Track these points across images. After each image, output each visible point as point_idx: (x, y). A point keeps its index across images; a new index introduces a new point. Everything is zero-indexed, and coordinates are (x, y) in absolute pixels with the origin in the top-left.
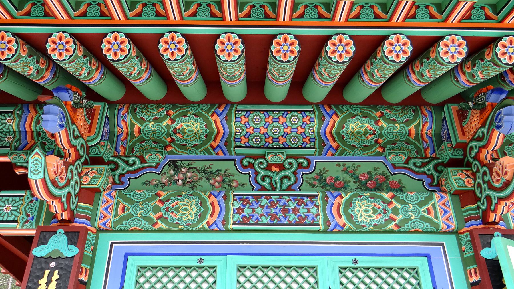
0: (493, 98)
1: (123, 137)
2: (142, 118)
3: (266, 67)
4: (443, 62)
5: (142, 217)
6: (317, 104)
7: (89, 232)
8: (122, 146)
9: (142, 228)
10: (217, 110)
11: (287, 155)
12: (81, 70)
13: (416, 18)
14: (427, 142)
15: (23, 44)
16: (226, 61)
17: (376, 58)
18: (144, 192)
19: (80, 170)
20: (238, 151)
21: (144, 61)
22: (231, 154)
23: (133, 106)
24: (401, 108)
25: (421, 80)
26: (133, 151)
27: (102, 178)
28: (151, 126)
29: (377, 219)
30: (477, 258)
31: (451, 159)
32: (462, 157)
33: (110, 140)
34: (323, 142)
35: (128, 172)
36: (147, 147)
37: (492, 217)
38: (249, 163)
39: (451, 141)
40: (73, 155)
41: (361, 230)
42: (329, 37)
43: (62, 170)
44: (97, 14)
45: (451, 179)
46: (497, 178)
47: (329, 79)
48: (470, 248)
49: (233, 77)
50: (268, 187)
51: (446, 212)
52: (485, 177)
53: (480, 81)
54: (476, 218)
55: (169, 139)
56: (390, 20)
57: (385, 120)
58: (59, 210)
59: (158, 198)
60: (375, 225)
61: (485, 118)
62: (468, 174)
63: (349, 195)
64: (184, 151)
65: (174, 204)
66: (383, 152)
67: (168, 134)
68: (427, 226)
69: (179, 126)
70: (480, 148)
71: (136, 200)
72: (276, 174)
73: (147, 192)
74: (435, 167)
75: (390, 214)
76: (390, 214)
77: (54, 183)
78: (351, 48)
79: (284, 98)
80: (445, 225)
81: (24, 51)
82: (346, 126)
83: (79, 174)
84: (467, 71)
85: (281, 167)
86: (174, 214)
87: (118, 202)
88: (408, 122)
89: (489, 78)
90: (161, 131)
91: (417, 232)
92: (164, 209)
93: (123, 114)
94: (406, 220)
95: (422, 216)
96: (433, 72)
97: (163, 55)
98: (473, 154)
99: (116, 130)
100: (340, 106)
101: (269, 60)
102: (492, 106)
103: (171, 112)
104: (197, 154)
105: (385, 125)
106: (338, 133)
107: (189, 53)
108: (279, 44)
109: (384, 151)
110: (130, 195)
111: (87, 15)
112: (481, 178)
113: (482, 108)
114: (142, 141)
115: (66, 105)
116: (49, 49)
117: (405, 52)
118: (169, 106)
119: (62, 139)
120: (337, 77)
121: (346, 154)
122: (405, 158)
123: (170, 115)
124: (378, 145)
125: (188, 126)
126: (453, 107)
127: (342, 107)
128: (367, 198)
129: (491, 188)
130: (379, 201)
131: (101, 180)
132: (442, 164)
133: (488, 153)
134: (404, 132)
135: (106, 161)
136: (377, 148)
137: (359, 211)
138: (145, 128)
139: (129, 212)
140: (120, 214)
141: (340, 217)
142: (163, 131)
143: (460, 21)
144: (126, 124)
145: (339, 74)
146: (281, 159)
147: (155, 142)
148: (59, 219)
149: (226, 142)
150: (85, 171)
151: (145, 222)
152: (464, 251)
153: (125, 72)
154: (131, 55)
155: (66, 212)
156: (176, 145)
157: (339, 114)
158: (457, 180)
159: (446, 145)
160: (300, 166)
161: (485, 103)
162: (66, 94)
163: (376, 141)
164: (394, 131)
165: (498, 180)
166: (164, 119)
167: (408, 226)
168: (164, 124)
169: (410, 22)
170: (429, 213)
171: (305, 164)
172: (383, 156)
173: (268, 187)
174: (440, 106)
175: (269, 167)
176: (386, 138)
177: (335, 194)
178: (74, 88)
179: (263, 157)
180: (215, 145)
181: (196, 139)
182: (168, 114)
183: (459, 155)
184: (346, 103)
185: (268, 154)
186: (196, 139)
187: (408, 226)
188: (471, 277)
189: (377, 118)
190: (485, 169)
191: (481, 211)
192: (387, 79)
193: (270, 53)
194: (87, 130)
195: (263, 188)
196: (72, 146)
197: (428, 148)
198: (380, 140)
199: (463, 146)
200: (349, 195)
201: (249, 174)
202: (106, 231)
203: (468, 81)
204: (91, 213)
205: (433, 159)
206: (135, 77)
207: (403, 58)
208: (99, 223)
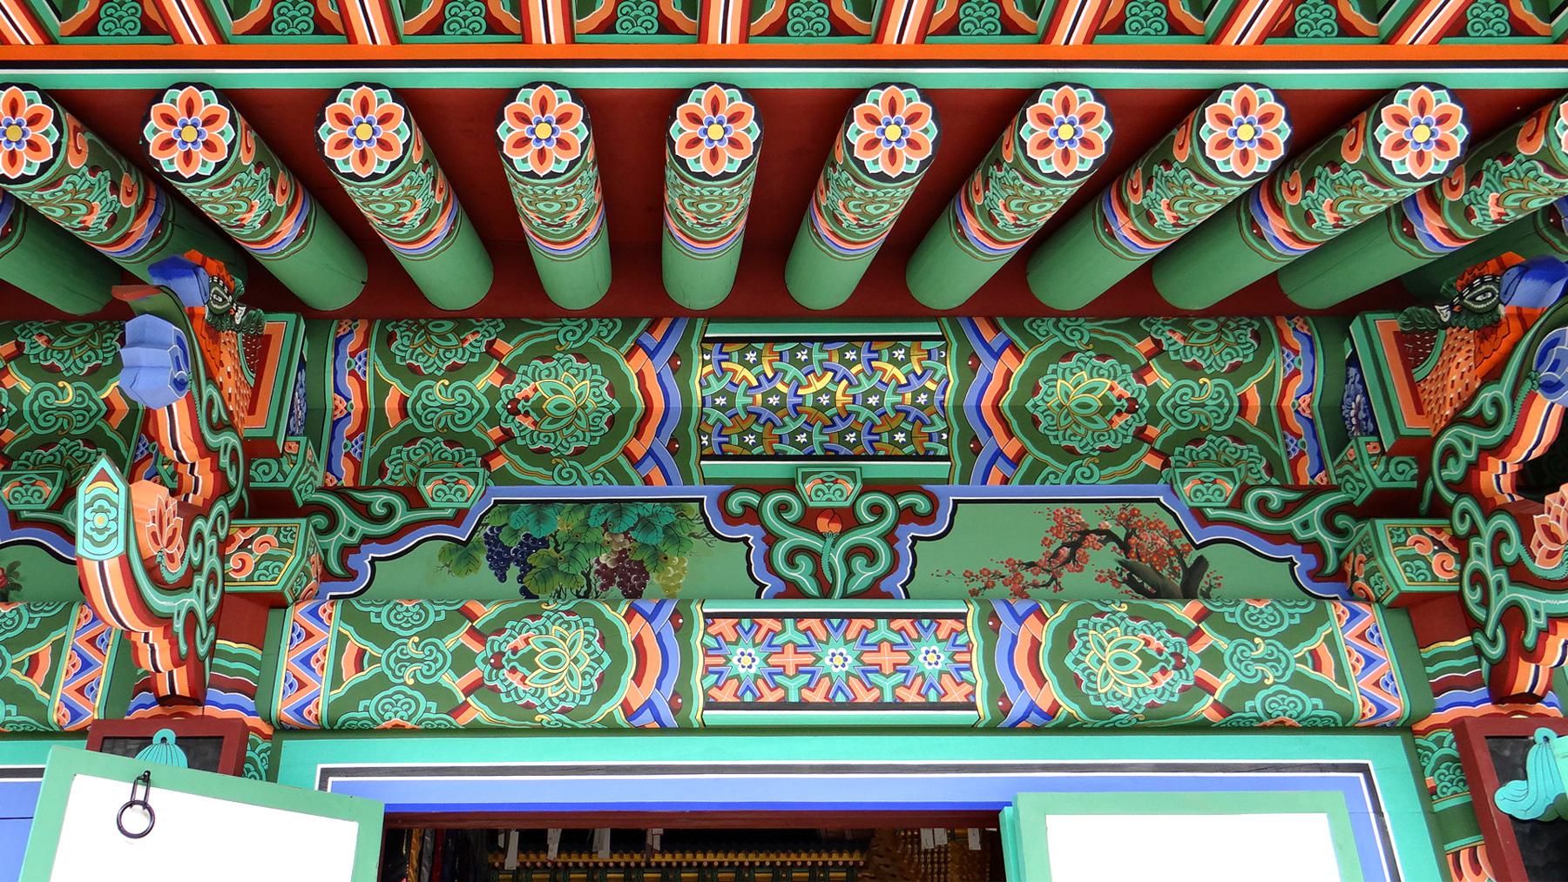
0: (1527, 292)
1: (350, 427)
2: (410, 366)
3: (662, 200)
4: (1215, 174)
5: (417, 686)
6: (952, 315)
7: (252, 736)
8: (348, 455)
11: (864, 481)
13: (1466, 35)
14: (1298, 436)
15: (76, 130)
16: (532, 174)
17: (999, 163)
19: (222, 534)
20: (713, 468)
21: (283, 180)
23: (383, 327)
24: (1214, 326)
25: (1146, 232)
26: (382, 471)
27: (293, 559)
28: (439, 392)
29: (1163, 688)
31: (1378, 494)
32: (1414, 484)
33: (314, 436)
35: (367, 539)
36: (427, 459)
37: (1525, 677)
38: (745, 505)
39: (1376, 432)
40: (206, 482)
41: (1107, 724)
42: (1031, 95)
43: (175, 530)
44: (304, 26)
45: (1388, 559)
46: (1548, 546)
48: (1451, 781)
49: (715, 230)
50: (810, 586)
51: (1370, 661)
52: (1504, 547)
53: (1488, 228)
55: (495, 432)
56: (1217, 38)
57: (1169, 367)
58: (164, 660)
59: (468, 624)
60: (1152, 705)
62: (1444, 539)
63: (1064, 611)
64: (541, 470)
65: (519, 642)
67: (492, 418)
69: (527, 390)
70: (1486, 451)
71: (397, 630)
72: (830, 541)
73: (29, 610)
75: (1195, 669)
76: (1195, 669)
77: (152, 570)
78: (748, 130)
79: (842, 300)
80: (1371, 705)
81: (79, 152)
82: (1044, 387)
84: (1289, 203)
85: (847, 519)
87: (342, 640)
88: (1237, 372)
89: (1357, 222)
90: (470, 407)
91: (1280, 728)
93: (353, 355)
94: (1243, 691)
95: (1297, 674)
96: (1348, 206)
98: (1455, 471)
99: (330, 406)
100: (1026, 324)
101: (668, 173)
102: (1524, 319)
103: (501, 346)
104: (584, 482)
105: (26, 386)
106: (1017, 408)
107: (590, 153)
108: (523, 118)
109: (1166, 464)
110: (378, 615)
111: (274, 31)
112: (1487, 553)
113: (1487, 326)
116: (152, 140)
117: (1087, 144)
118: (495, 327)
120: (887, 224)
121: (1046, 478)
122: (1230, 488)
123: (499, 356)
124: (1146, 446)
125: (556, 392)
126: (1384, 325)
128: (1122, 619)
129: (1520, 575)
130: (1159, 629)
131: (287, 568)
132: (1345, 508)
133: (1504, 472)
134: (1227, 404)
135: (300, 504)
138: (418, 398)
140: (351, 679)
141: (1041, 681)
142: (477, 406)
143: (1261, 41)
144: (363, 385)
145: (891, 217)
146: (842, 493)
147: (451, 443)
149: (673, 440)
151: (430, 704)
152: (1433, 791)
153: (223, 216)
158: (1405, 559)
159: (1362, 446)
161: (1494, 308)
163: (1140, 435)
164: (1195, 401)
166: (481, 368)
168: (482, 383)
169: (1109, 45)
170: (1317, 667)
173: (810, 586)
175: (808, 522)
177: (1021, 607)
178: (213, 265)
179: (790, 486)
180: (638, 449)
182: (491, 352)
183: (1402, 475)
184: (1045, 312)
185: (806, 476)
190: (1503, 521)
191: (1485, 663)
192: (1034, 230)
193: (668, 150)
194: (246, 404)
195: (793, 591)
197: (1302, 454)
198: (1152, 431)
199: (1419, 450)
200: (1064, 611)
201: (745, 540)
203: (1293, 236)
204: (256, 673)
205: (1313, 492)
206: (255, 233)
207: (1085, 161)
208: (282, 706)
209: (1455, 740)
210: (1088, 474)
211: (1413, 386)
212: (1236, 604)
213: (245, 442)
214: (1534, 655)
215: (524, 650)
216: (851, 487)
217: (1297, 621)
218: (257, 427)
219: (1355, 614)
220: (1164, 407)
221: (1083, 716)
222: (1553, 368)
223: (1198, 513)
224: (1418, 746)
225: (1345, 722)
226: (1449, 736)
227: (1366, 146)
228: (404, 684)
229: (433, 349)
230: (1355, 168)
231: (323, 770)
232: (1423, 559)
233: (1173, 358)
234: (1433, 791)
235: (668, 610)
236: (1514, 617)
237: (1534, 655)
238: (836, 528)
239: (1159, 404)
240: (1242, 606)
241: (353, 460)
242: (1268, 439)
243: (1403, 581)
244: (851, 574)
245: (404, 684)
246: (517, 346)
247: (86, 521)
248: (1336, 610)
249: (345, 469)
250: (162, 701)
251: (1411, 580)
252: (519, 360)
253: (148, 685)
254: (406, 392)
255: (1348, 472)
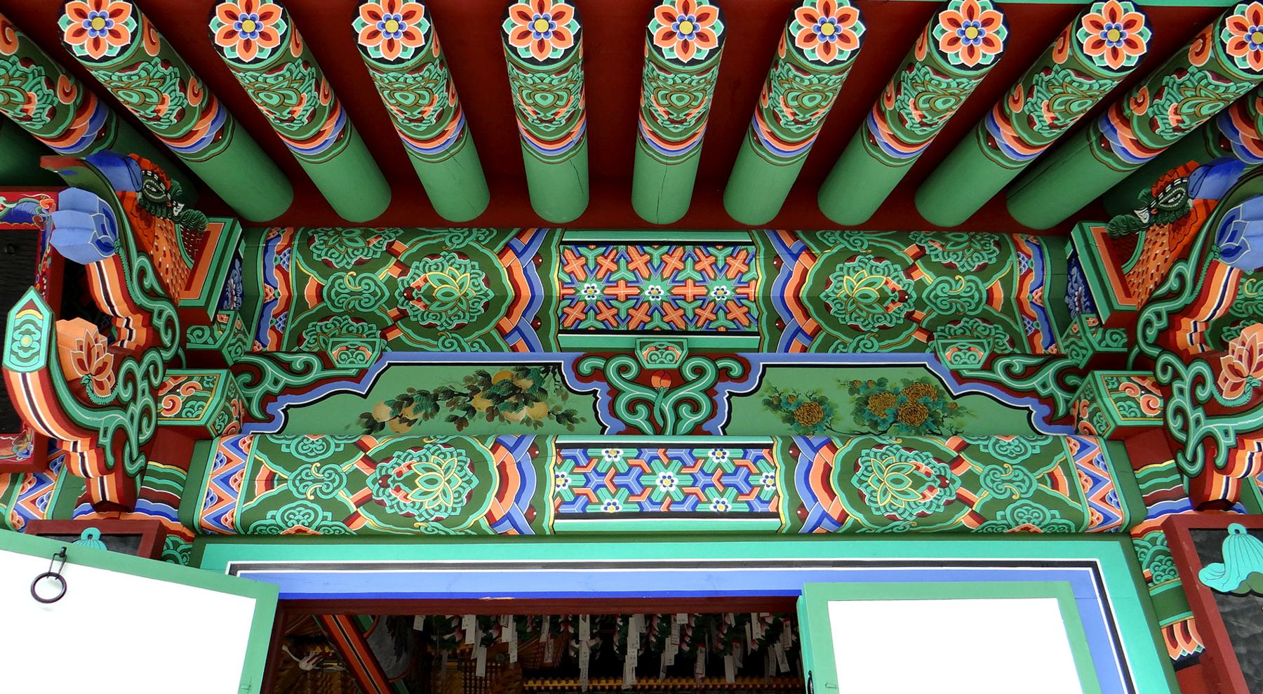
5: (317, 500)
6: (759, 228)
8: (273, 328)
9: (318, 529)
10: (515, 242)
12: (155, 99)
14: (1034, 319)
18: (324, 440)
19: (156, 383)
20: (567, 340)
22: (547, 348)
24: (966, 237)
26: (300, 340)
29: (930, 501)
30: (1190, 595)
32: (1125, 350)
34: (779, 320)
35: (288, 390)
36: (337, 331)
37: (1220, 488)
39: (1093, 309)
41: (886, 530)
45: (1106, 400)
46: (1233, 380)
47: (794, 128)
54: (1177, 495)
55: (394, 312)
57: (930, 266)
59: (362, 454)
60: (922, 515)
61: (1187, 239)
66: (928, 340)
68: (1053, 517)
72: (662, 394)
74: (1060, 377)
75: (958, 488)
76: (958, 488)
80: (1098, 514)
83: (154, 391)
85: (677, 379)
86: (402, 493)
87: (257, 465)
91: (1027, 534)
92: (374, 482)
93: (279, 253)
94: (995, 505)
96: (1060, 105)
97: (364, 49)
103: (399, 246)
105: (928, 277)
106: (813, 298)
109: (930, 338)
110: (288, 446)
113: (1179, 219)
114: (325, 316)
115: (122, 199)
119: (106, 283)
122: (983, 355)
123: (396, 254)
125: (442, 282)
126: (1094, 229)
127: (822, 235)
128: (898, 450)
129: (1214, 409)
132: (1073, 370)
134: (977, 296)
136: (913, 333)
137: (880, 481)
138: (332, 286)
139: (283, 487)
140: (261, 494)
141: (832, 495)
144: (286, 275)
146: (673, 357)
147: (357, 320)
148: (96, 501)
150: (172, 384)
151: (326, 514)
154: (287, 50)
155: (112, 476)
156: (409, 325)
157: (816, 251)
158: (1123, 401)
160: (723, 374)
161: (1184, 204)
162: (123, 171)
163: (909, 316)
165: (1235, 387)
166: (382, 263)
167: (1004, 517)
168: (383, 275)
170: (1055, 485)
171: (737, 370)
172: (928, 350)
173: (646, 427)
174: (1061, 232)
175: (644, 378)
176: (932, 310)
179: (631, 353)
180: (508, 325)
181: (460, 313)
182: (391, 252)
183: (1115, 342)
184: (833, 226)
185: (643, 345)
186: (460, 313)
187: (1004, 517)
188: (1175, 644)
189: (910, 262)
191: (1185, 477)
195: (634, 430)
196: (136, 308)
197: (1037, 332)
198: (919, 314)
199: (1125, 322)
201: (595, 392)
202: (220, 536)
204: (181, 489)
208: (203, 514)
209: (1166, 538)
210: (869, 345)
211: (1122, 278)
212: (989, 438)
213: (181, 311)
214: (1226, 469)
215: (407, 473)
216: (679, 352)
217: (1037, 451)
218: (189, 300)
219: (1084, 447)
220: (928, 297)
221: (866, 522)
222: (1231, 239)
223: (956, 374)
224: (1134, 545)
225: (1078, 528)
226: (1160, 535)
227: (1071, 46)
228: (306, 499)
229: (343, 249)
230: (1063, 67)
231: (232, 566)
232: (1133, 399)
233: (934, 260)
234: (1150, 580)
235: (527, 443)
236: (1209, 442)
237: (1226, 469)
238: (667, 383)
239: (924, 296)
240: (993, 440)
241: (277, 332)
242: (1012, 323)
243: (1118, 416)
244: (678, 418)
245: (306, 499)
246: (412, 246)
247: (14, 340)
248: (1070, 445)
249: (270, 338)
250: (98, 507)
251: (1124, 416)
252: (414, 257)
253: (87, 498)
254: (323, 282)
255: (1073, 343)
